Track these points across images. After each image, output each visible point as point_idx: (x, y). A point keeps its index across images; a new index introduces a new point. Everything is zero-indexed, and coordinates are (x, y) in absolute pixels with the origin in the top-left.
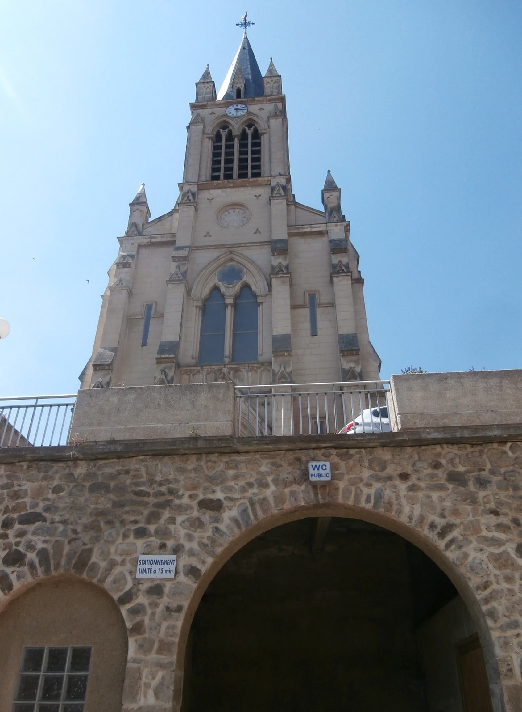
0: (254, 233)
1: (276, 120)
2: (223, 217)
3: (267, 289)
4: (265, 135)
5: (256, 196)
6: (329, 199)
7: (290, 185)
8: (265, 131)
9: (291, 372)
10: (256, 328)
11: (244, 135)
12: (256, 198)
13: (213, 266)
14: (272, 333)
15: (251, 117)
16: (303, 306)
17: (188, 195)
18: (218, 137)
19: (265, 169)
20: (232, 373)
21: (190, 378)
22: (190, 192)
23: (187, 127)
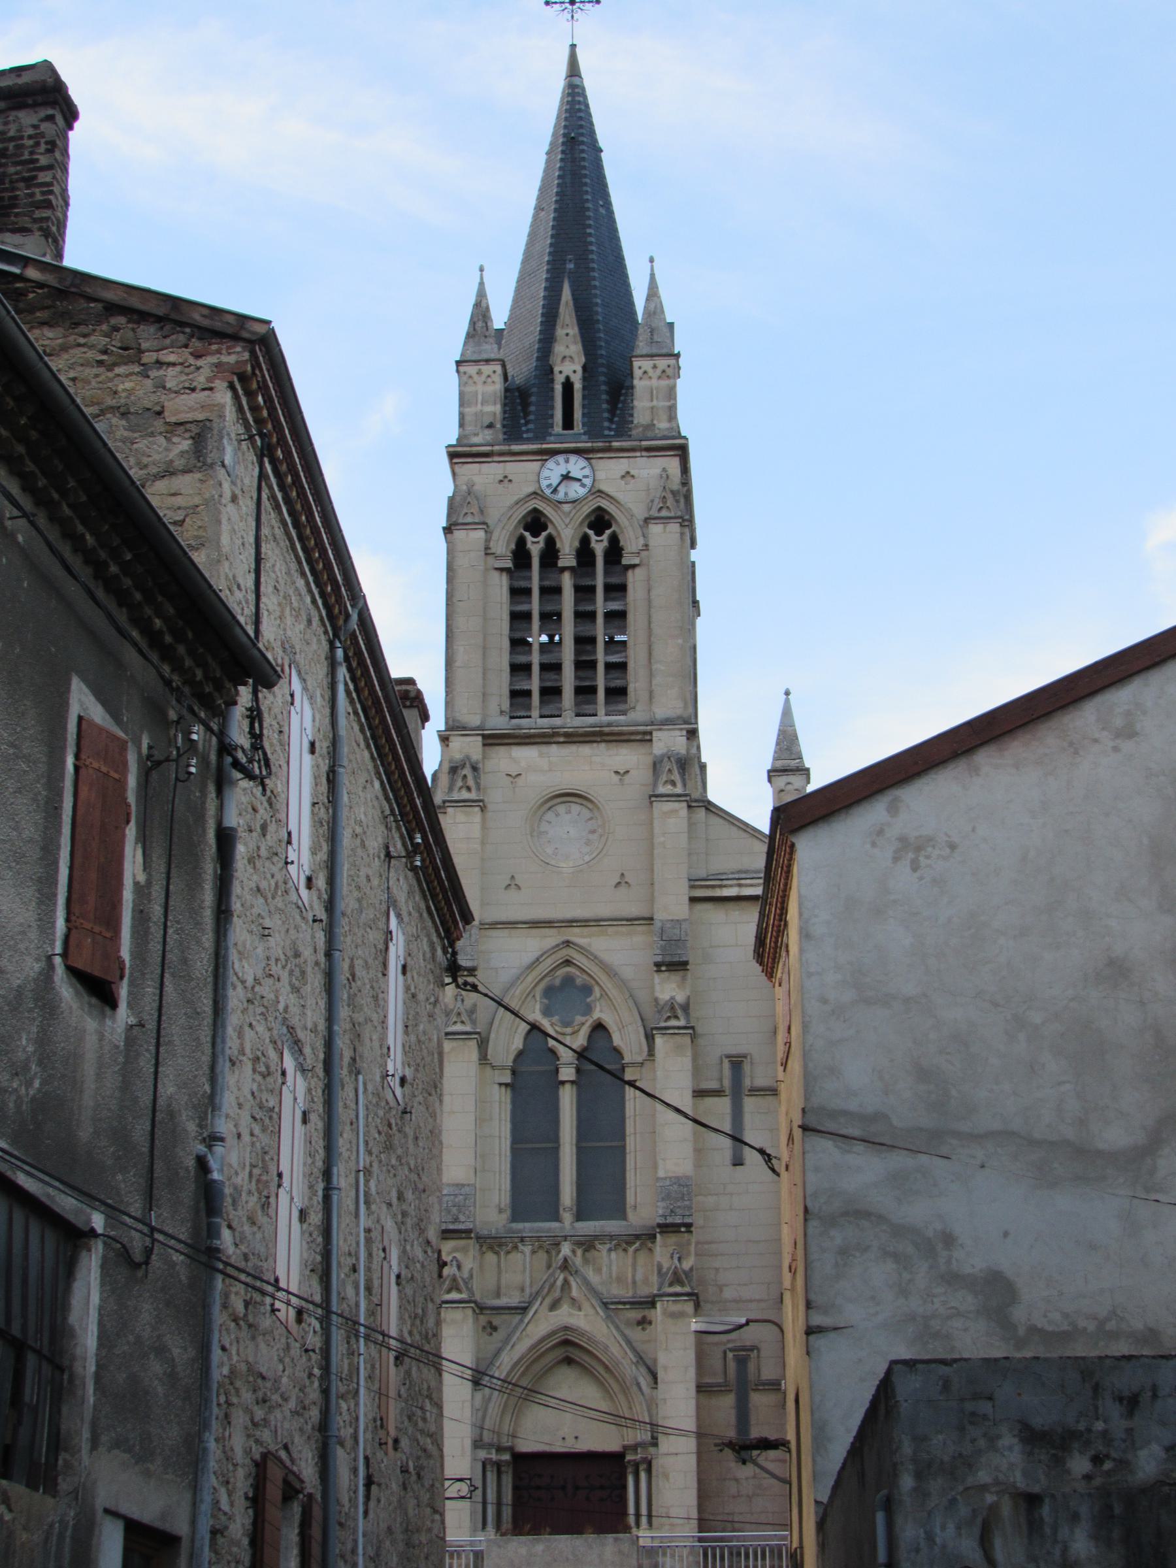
0: (616, 887)
1: (665, 527)
2: (544, 827)
3: (645, 1049)
4: (637, 571)
5: (617, 773)
6: (783, 793)
7: (695, 744)
8: (636, 561)
9: (691, 1269)
10: (623, 1137)
11: (585, 553)
12: (616, 778)
13: (530, 979)
14: (655, 1167)
15: (604, 504)
16: (717, 1093)
17: (464, 773)
18: (521, 555)
19: (636, 683)
20: (579, 1252)
21: (499, 1262)
22: (468, 765)
23: (444, 529)
